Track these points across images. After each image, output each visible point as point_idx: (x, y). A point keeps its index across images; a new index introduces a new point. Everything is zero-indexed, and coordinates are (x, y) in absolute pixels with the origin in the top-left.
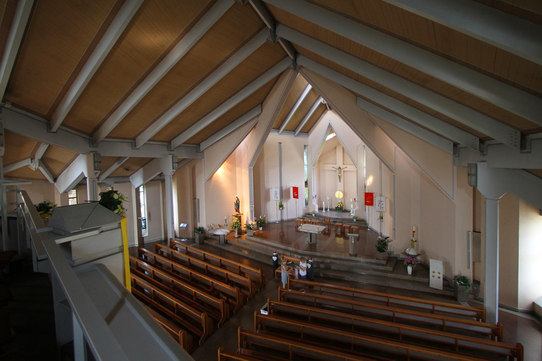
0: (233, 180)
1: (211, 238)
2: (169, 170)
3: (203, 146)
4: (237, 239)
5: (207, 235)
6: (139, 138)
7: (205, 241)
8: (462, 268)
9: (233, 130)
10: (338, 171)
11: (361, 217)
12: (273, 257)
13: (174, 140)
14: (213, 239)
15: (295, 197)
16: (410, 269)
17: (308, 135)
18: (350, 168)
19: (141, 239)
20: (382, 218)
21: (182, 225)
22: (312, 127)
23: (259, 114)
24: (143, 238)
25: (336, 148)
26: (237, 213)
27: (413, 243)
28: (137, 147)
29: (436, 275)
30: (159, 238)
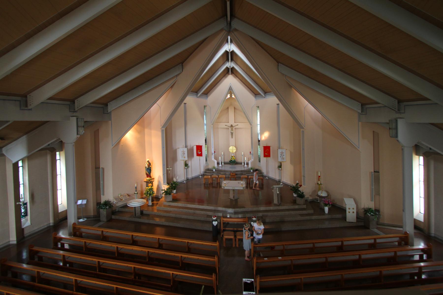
0: (141, 142)
1: (119, 211)
2: (71, 134)
3: (111, 107)
4: (150, 208)
5: (114, 209)
6: (32, 94)
7: (113, 217)
8: (367, 202)
9: (149, 89)
10: (230, 129)
12: (214, 222)
13: (79, 99)
14: (121, 212)
15: (198, 155)
16: (326, 209)
17: (207, 97)
18: (242, 125)
19: (20, 230)
20: (280, 166)
21: (80, 202)
23: (179, 74)
24: (23, 229)
25: (228, 108)
26: (148, 178)
27: (319, 186)
28: (30, 107)
29: (351, 211)
30: (46, 224)
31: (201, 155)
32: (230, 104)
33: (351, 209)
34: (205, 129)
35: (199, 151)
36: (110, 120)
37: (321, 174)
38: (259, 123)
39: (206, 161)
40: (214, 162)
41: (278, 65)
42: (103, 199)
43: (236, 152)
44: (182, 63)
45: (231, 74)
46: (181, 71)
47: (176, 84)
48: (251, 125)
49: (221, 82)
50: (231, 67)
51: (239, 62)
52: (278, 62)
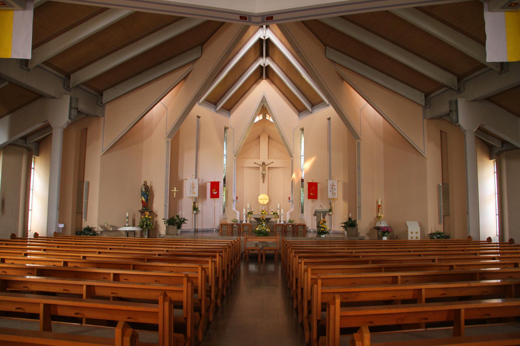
2: (61, 117)
3: (107, 96)
10: (261, 168)
11: (297, 222)
15: (213, 196)
17: (230, 114)
22: (237, 102)
31: (217, 196)
32: (263, 132)
33: (414, 233)
34: (225, 163)
35: (214, 190)
36: (104, 116)
37: (381, 202)
38: (302, 154)
39: (224, 211)
40: (236, 212)
41: (326, 49)
42: (85, 225)
44: (202, 44)
45: (266, 79)
46: (200, 54)
47: (191, 74)
48: (292, 156)
49: (252, 91)
51: (276, 58)
52: (325, 45)
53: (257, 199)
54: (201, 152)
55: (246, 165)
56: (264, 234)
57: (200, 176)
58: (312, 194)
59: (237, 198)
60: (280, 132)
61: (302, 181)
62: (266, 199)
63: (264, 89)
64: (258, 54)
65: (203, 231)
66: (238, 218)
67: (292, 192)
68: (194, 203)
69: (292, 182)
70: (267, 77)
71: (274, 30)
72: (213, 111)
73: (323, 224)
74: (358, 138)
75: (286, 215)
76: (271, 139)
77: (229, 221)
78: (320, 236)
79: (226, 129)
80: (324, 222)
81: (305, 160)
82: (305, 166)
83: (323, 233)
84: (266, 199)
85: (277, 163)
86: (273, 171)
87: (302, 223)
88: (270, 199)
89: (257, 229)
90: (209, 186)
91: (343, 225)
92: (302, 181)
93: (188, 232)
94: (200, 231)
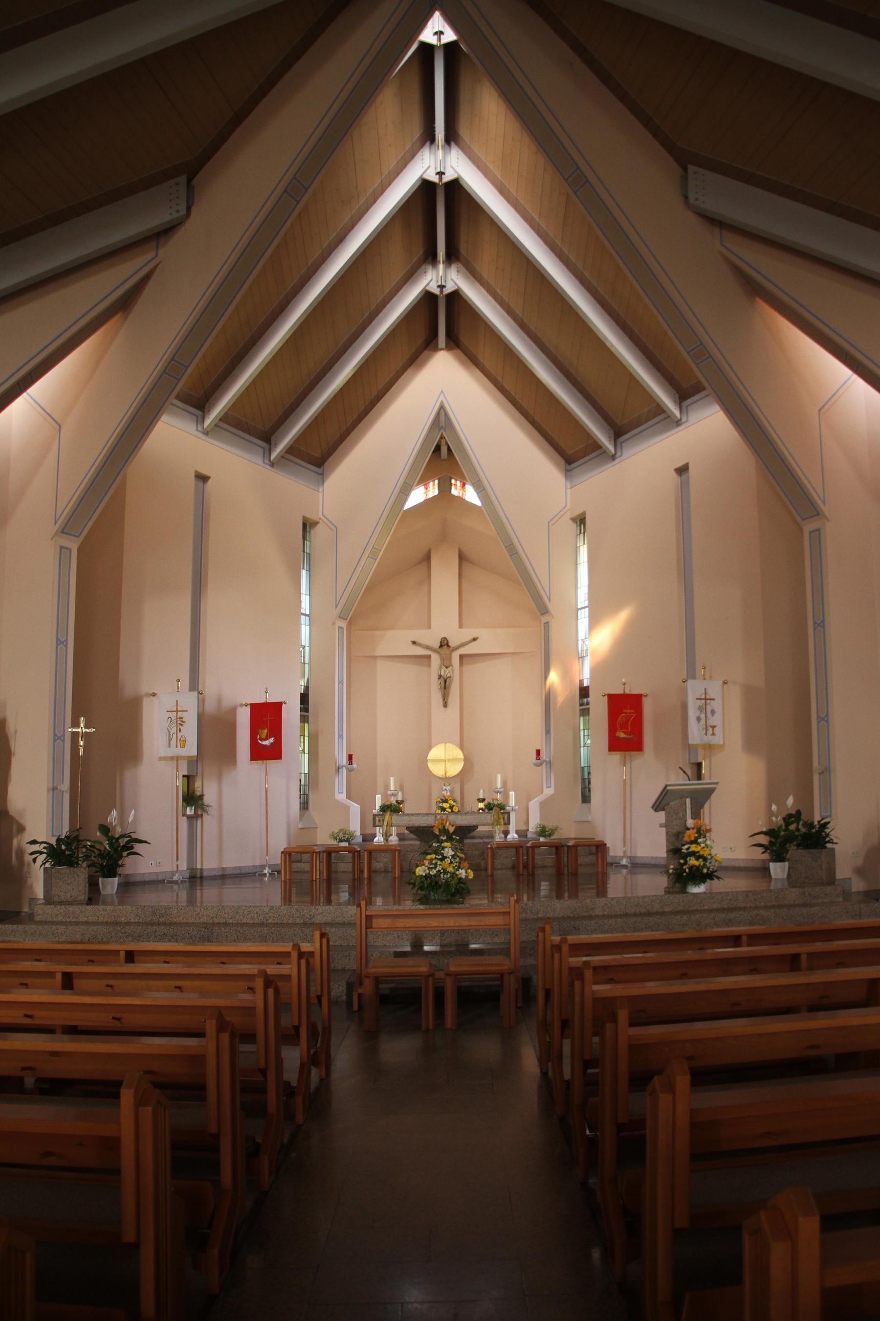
10: (435, 659)
11: (568, 832)
15: (259, 753)
17: (322, 477)
31: (275, 753)
39: (304, 806)
40: (347, 809)
43: (462, 776)
45: (448, 348)
46: (183, 212)
48: (544, 611)
50: (449, 289)
51: (485, 353)
52: (684, 159)
53: (425, 761)
54: (212, 602)
55: (382, 650)
56: (451, 892)
57: (210, 684)
58: (622, 735)
59: (350, 757)
60: (501, 529)
61: (584, 692)
62: (454, 760)
63: (442, 382)
64: (419, 251)
65: (223, 877)
66: (355, 827)
67: (548, 732)
68: (189, 779)
69: (548, 699)
70: (454, 342)
71: (475, 148)
72: (260, 461)
73: (695, 842)
74: (816, 513)
75: (531, 809)
76: (470, 562)
77: (323, 839)
78: (683, 891)
79: (307, 526)
80: (701, 832)
81: (594, 623)
82: (594, 641)
83: (699, 876)
84: (454, 760)
85: (488, 641)
86: (475, 670)
87: (587, 835)
88: (468, 761)
89: (420, 871)
90: (244, 718)
91: (764, 840)
92: (584, 692)
93: (162, 882)
94: (213, 878)
